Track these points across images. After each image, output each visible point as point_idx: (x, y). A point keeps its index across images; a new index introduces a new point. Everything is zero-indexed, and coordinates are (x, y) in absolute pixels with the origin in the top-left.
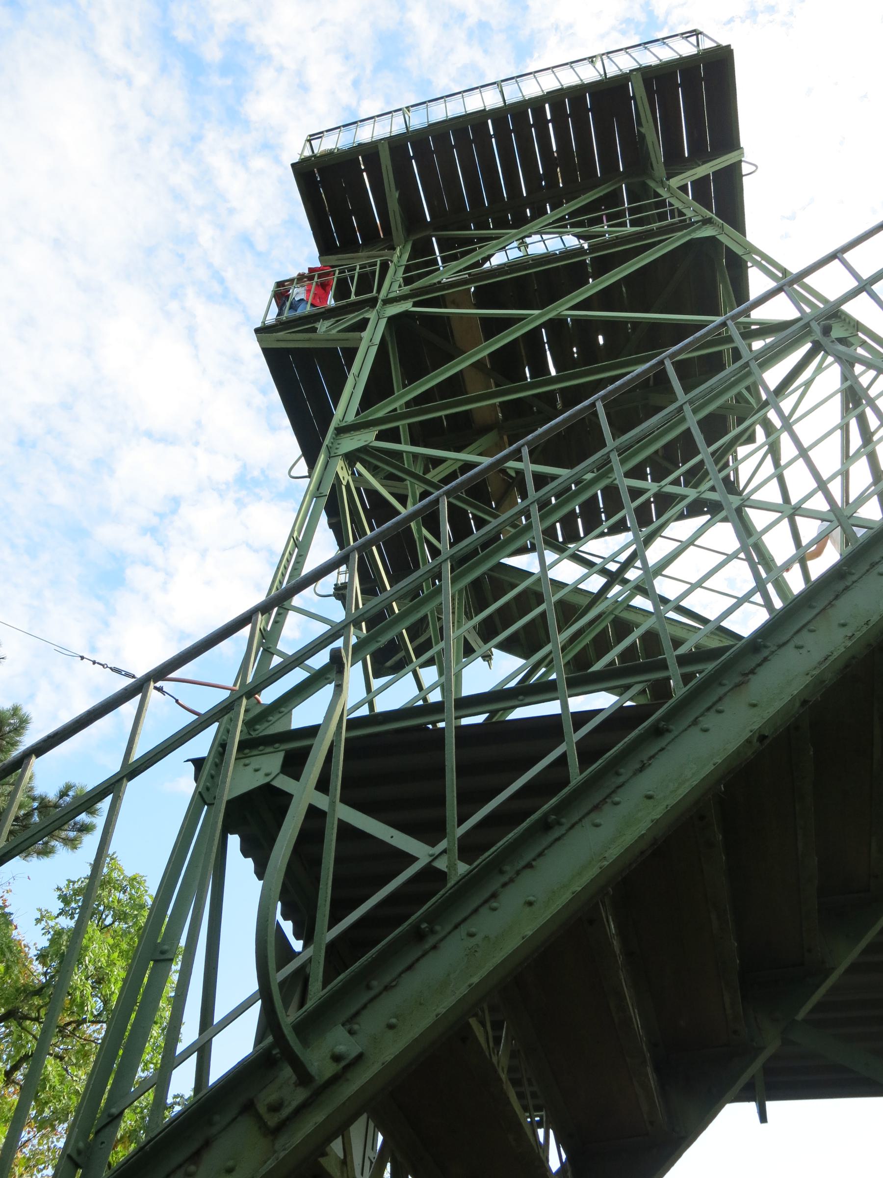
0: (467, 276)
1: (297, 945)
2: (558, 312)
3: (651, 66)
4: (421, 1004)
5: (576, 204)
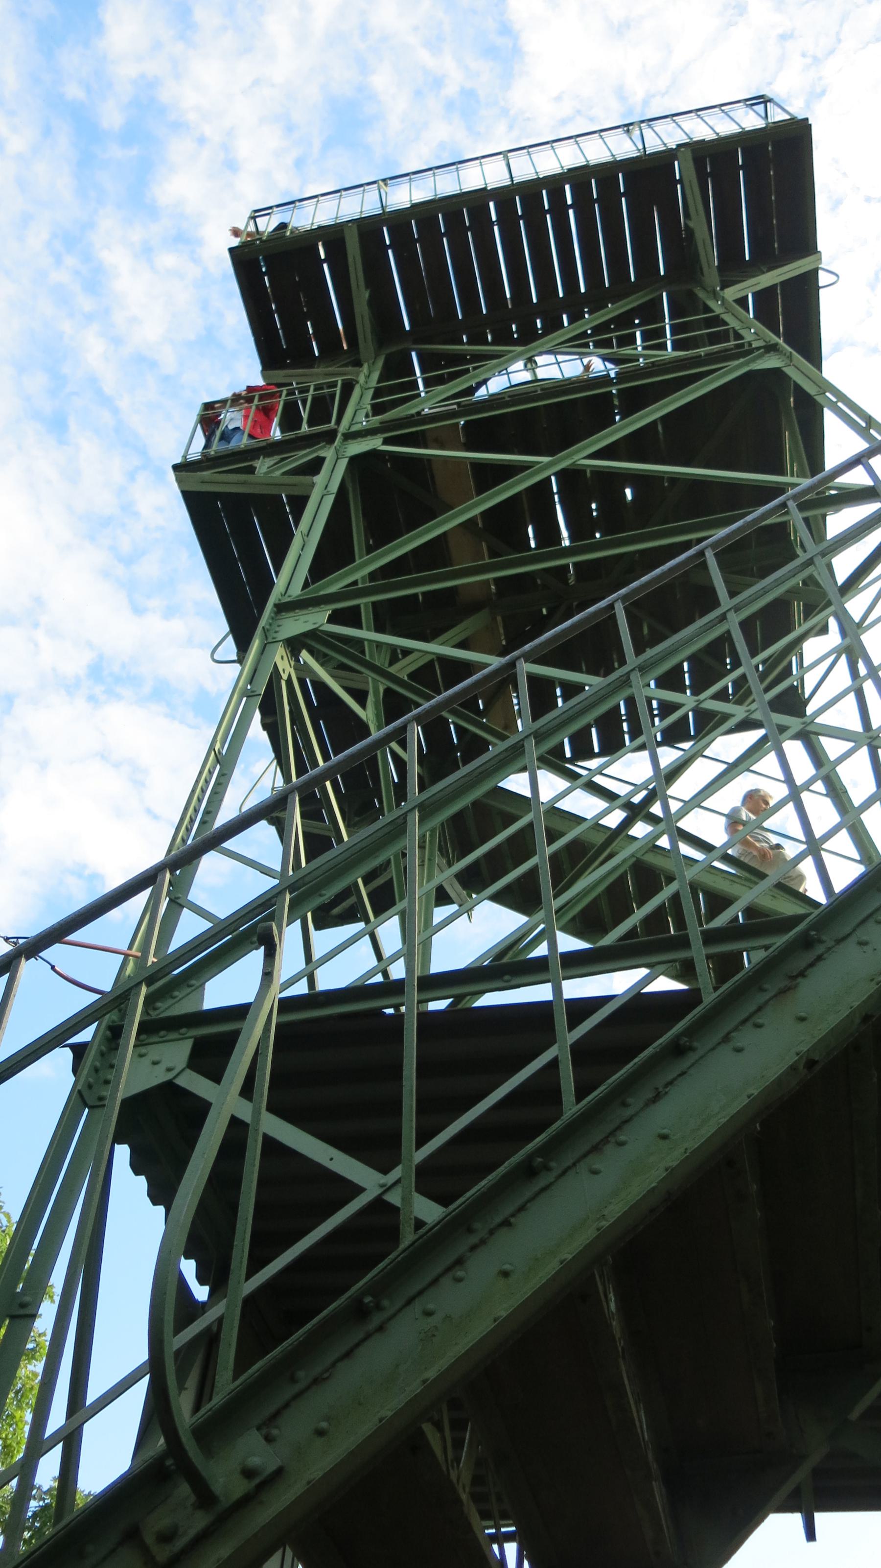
0: (455, 407)
1: (201, 1293)
2: (573, 461)
3: (703, 141)
4: (360, 1404)
5: (603, 315)
